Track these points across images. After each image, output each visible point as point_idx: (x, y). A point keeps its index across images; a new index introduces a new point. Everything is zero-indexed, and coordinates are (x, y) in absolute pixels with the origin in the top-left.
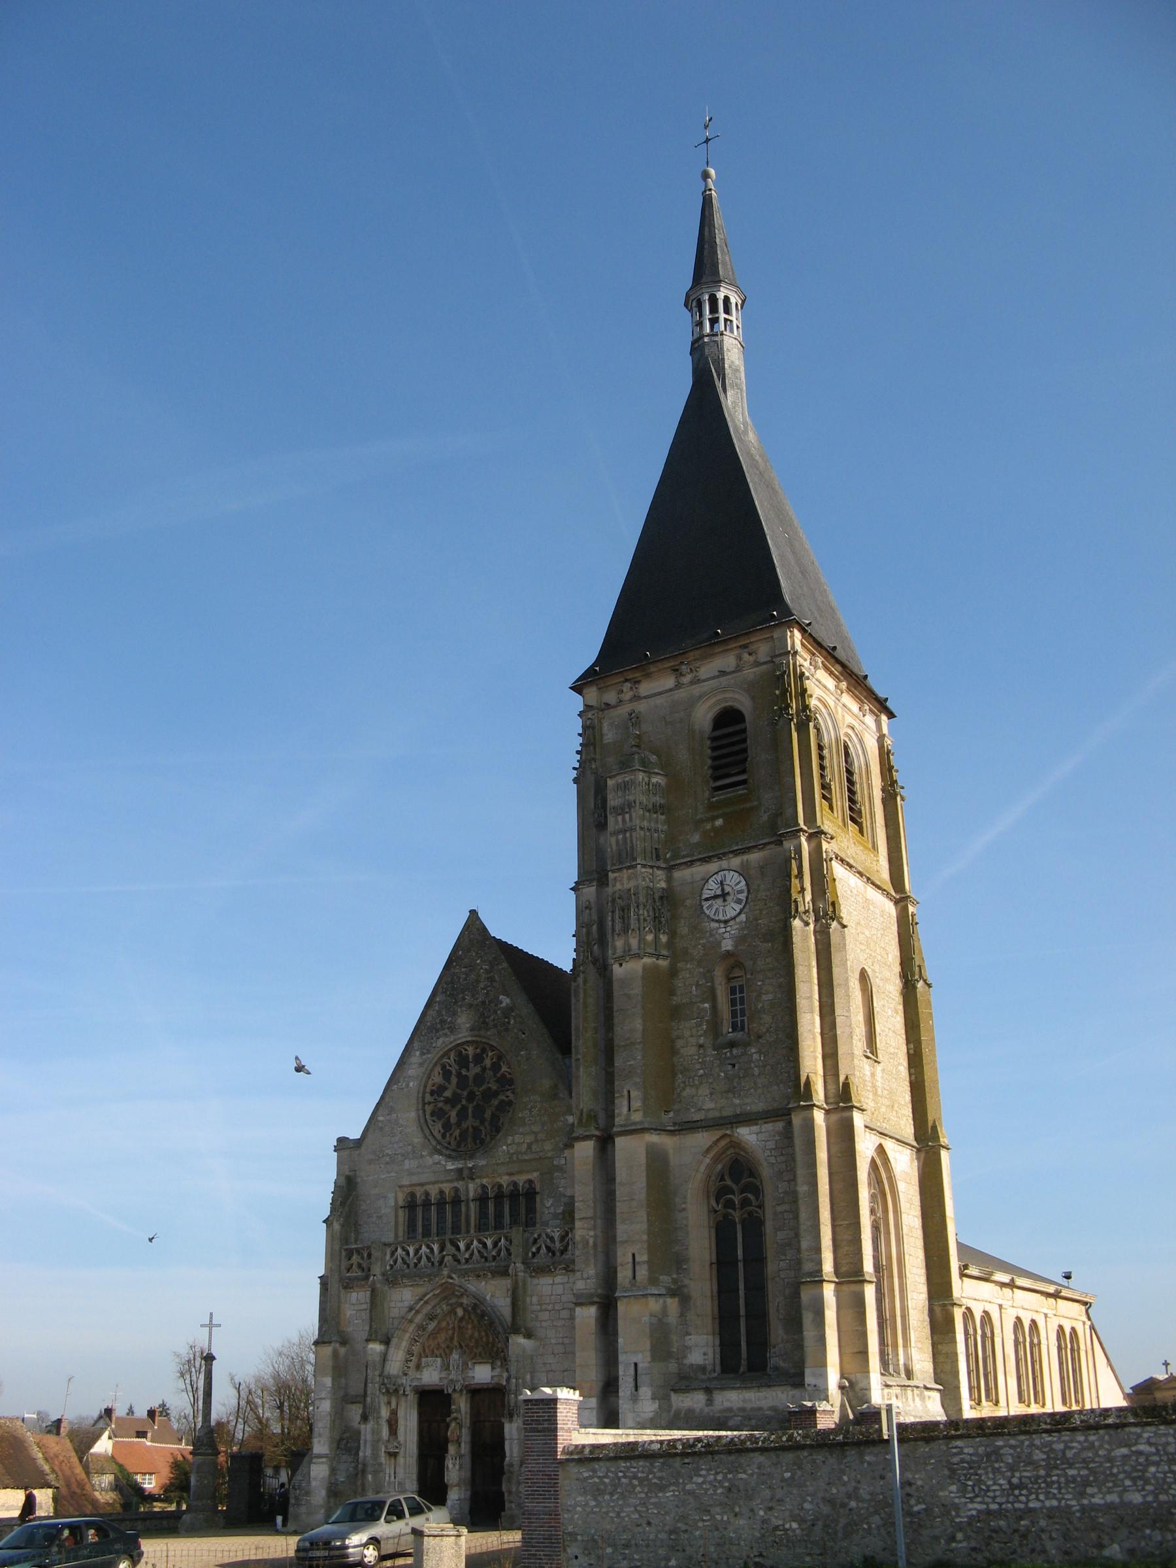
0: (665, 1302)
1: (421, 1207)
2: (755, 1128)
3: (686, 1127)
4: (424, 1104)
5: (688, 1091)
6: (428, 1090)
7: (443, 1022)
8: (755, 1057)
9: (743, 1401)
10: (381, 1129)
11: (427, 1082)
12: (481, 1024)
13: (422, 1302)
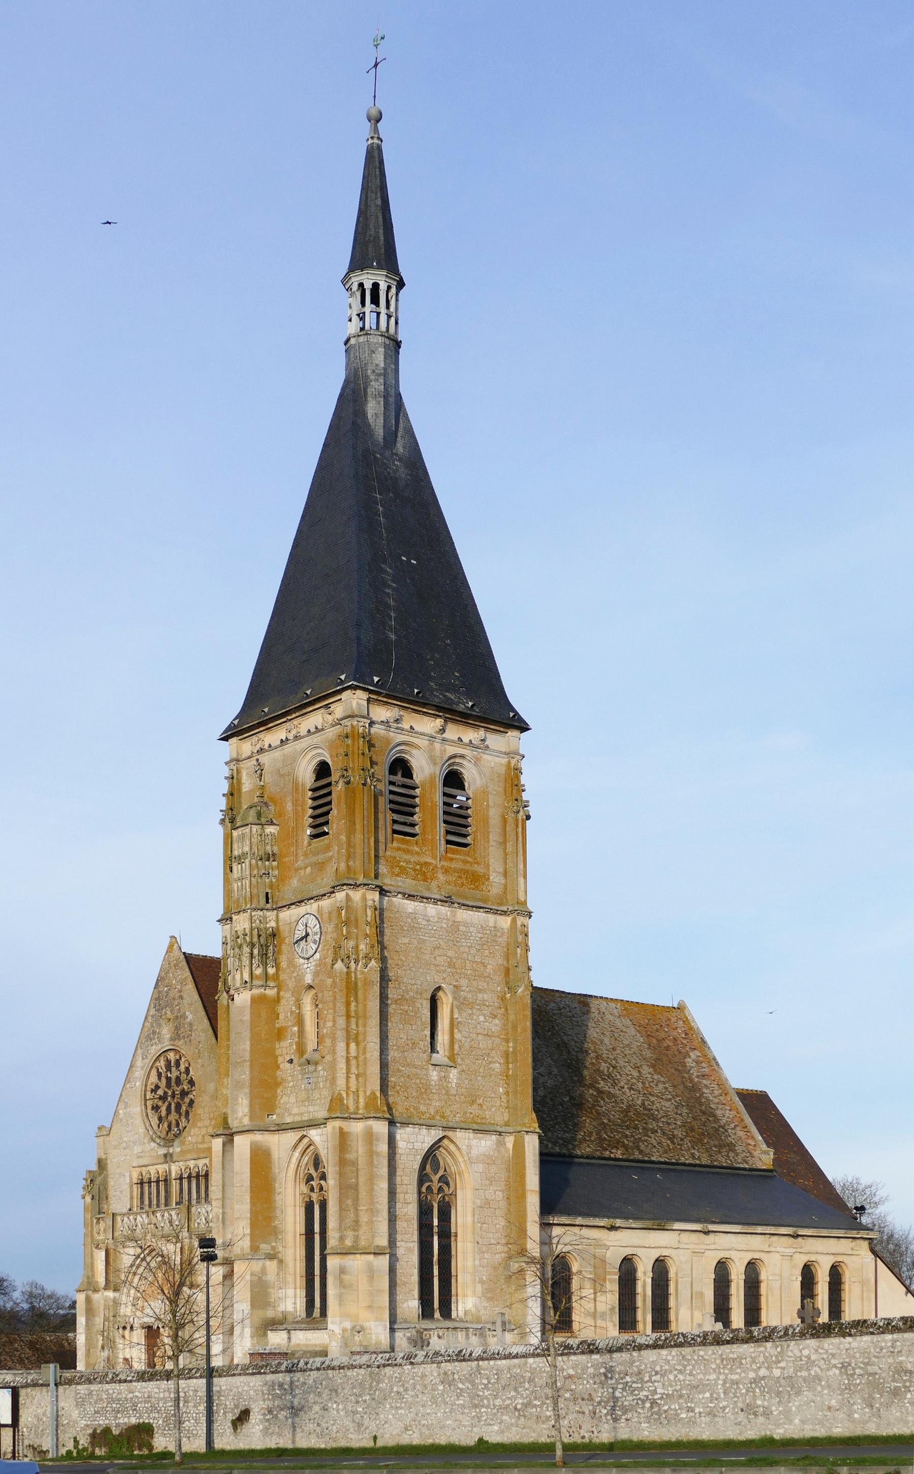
0: (264, 1264)
1: (163, 1183)
2: (319, 1131)
3: (281, 1128)
4: (146, 1100)
5: (285, 1099)
6: (149, 1089)
7: (154, 1032)
8: (321, 1073)
9: (306, 1339)
10: (121, 1120)
11: (147, 1082)
12: (176, 1036)
13: (139, 1259)
